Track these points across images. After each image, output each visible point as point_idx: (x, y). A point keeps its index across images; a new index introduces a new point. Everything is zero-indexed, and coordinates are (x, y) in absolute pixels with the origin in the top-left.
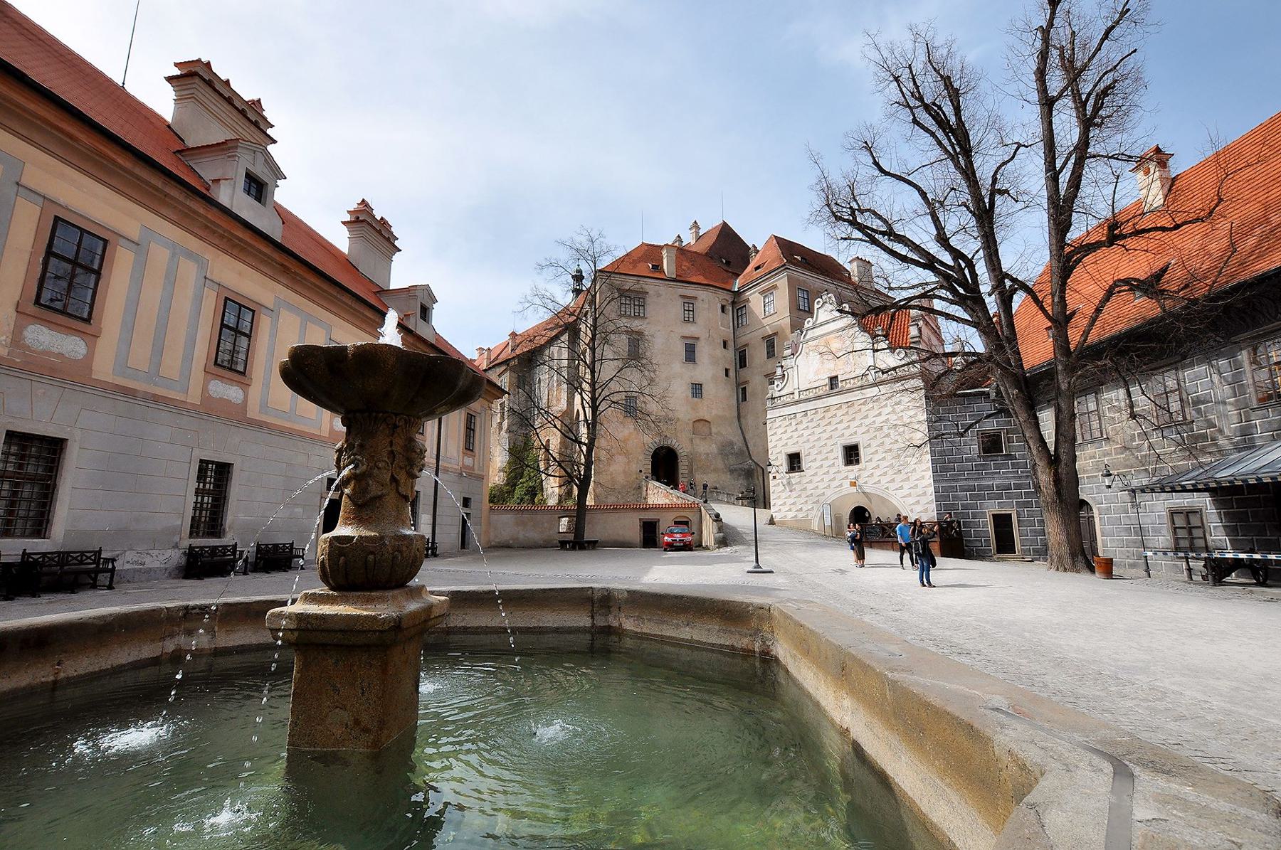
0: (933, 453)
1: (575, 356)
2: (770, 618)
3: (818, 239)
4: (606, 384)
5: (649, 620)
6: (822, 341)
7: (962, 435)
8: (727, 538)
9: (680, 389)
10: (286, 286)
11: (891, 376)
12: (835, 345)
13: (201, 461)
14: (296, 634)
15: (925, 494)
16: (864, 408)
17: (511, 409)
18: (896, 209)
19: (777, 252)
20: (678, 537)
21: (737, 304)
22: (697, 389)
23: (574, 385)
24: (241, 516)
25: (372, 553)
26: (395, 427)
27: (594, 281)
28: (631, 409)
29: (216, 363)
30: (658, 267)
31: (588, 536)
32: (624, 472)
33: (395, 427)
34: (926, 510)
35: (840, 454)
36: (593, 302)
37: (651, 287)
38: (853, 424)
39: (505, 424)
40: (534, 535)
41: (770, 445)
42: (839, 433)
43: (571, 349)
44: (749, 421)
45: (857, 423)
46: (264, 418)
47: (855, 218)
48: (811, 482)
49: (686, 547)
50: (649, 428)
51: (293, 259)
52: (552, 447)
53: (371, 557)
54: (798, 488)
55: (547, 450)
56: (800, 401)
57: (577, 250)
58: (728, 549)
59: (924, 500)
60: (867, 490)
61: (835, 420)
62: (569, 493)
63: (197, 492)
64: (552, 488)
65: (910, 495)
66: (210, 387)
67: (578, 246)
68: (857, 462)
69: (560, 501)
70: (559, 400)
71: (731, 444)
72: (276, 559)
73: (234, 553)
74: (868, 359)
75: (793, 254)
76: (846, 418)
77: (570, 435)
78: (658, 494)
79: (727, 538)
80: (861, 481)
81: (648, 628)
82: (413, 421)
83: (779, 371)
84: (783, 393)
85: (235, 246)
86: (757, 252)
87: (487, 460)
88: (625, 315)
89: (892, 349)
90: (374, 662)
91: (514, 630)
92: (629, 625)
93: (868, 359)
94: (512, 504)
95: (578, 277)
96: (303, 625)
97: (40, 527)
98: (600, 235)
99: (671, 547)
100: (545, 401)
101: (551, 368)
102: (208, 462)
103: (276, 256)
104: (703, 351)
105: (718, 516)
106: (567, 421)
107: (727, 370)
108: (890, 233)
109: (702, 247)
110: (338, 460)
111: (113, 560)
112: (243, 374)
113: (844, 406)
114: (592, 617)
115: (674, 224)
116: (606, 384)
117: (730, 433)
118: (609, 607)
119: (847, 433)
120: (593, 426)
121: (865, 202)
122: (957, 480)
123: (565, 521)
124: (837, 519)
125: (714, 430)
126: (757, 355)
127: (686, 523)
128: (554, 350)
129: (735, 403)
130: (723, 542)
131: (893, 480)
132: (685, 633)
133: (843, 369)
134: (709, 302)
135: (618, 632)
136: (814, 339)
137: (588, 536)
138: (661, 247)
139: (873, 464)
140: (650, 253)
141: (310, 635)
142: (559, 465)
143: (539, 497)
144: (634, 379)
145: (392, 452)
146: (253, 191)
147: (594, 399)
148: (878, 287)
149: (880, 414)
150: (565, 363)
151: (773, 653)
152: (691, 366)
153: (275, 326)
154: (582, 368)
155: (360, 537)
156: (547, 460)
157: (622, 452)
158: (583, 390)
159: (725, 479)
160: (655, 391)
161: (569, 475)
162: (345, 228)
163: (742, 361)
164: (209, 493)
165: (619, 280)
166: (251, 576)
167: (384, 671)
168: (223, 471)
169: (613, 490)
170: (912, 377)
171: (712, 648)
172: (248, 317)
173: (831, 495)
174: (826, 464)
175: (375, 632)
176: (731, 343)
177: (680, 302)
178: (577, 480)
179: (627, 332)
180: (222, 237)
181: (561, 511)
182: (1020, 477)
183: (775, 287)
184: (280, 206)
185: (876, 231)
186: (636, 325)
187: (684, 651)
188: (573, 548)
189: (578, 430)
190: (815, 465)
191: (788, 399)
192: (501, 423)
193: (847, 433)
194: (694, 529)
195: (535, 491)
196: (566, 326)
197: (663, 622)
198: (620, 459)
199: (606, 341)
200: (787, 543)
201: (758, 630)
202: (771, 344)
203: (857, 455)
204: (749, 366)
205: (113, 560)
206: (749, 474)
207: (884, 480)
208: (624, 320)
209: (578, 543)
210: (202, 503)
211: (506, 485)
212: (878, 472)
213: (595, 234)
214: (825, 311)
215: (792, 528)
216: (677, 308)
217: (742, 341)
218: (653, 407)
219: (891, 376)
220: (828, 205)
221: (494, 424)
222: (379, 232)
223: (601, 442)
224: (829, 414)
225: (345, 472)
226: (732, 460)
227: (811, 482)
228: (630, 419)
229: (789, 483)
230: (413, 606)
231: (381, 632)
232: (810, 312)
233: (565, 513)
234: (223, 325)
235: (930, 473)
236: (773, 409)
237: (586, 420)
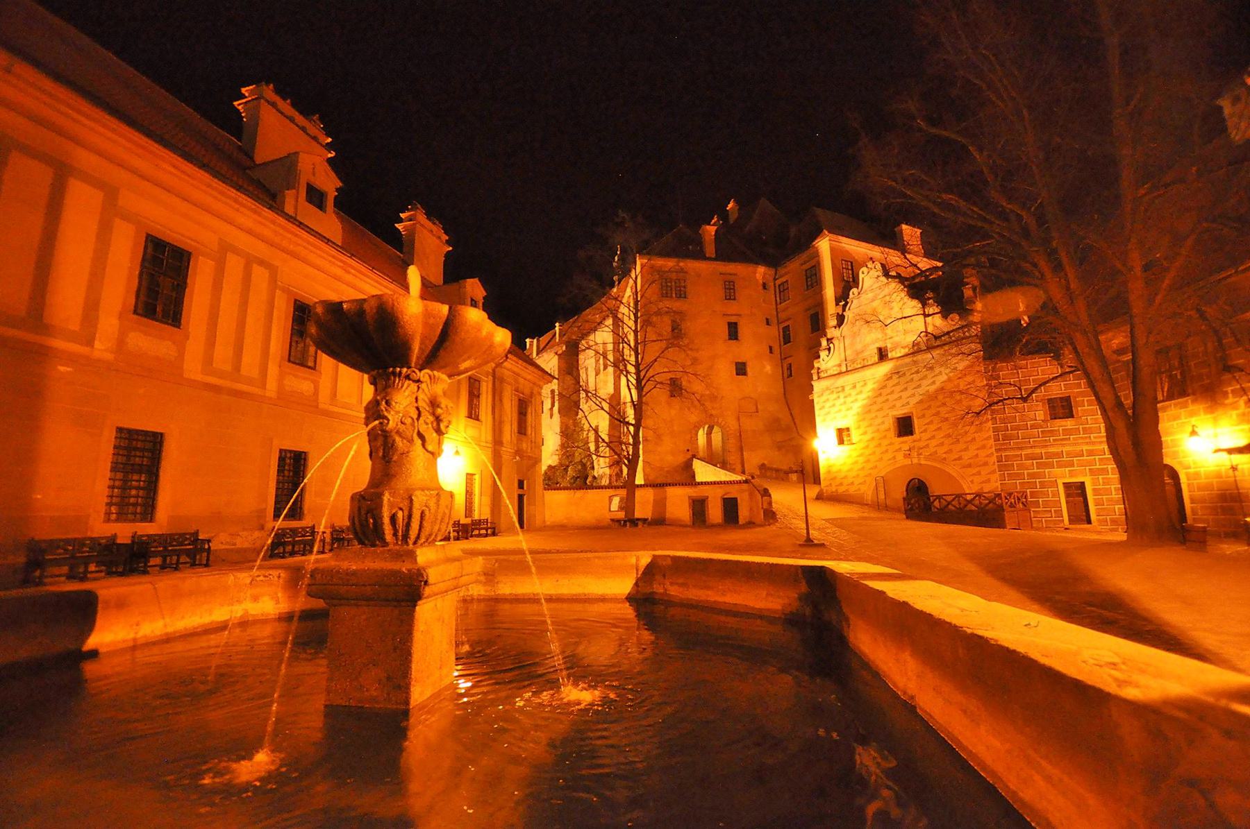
2: (906, 512)
7: (1025, 400)
13: (281, 451)
23: (619, 365)
43: (615, 333)
45: (909, 392)
52: (600, 429)
66: (286, 382)
76: (898, 388)
77: (617, 418)
87: (538, 444)
91: (550, 599)
92: (674, 591)
97: (148, 512)
101: (597, 352)
104: (744, 330)
106: (614, 403)
107: (771, 348)
111: (209, 541)
120: (638, 407)
122: (1021, 449)
147: (638, 380)
150: (610, 347)
154: (626, 351)
156: (597, 442)
158: (628, 372)
182: (1093, 443)
205: (209, 541)
218: (697, 387)
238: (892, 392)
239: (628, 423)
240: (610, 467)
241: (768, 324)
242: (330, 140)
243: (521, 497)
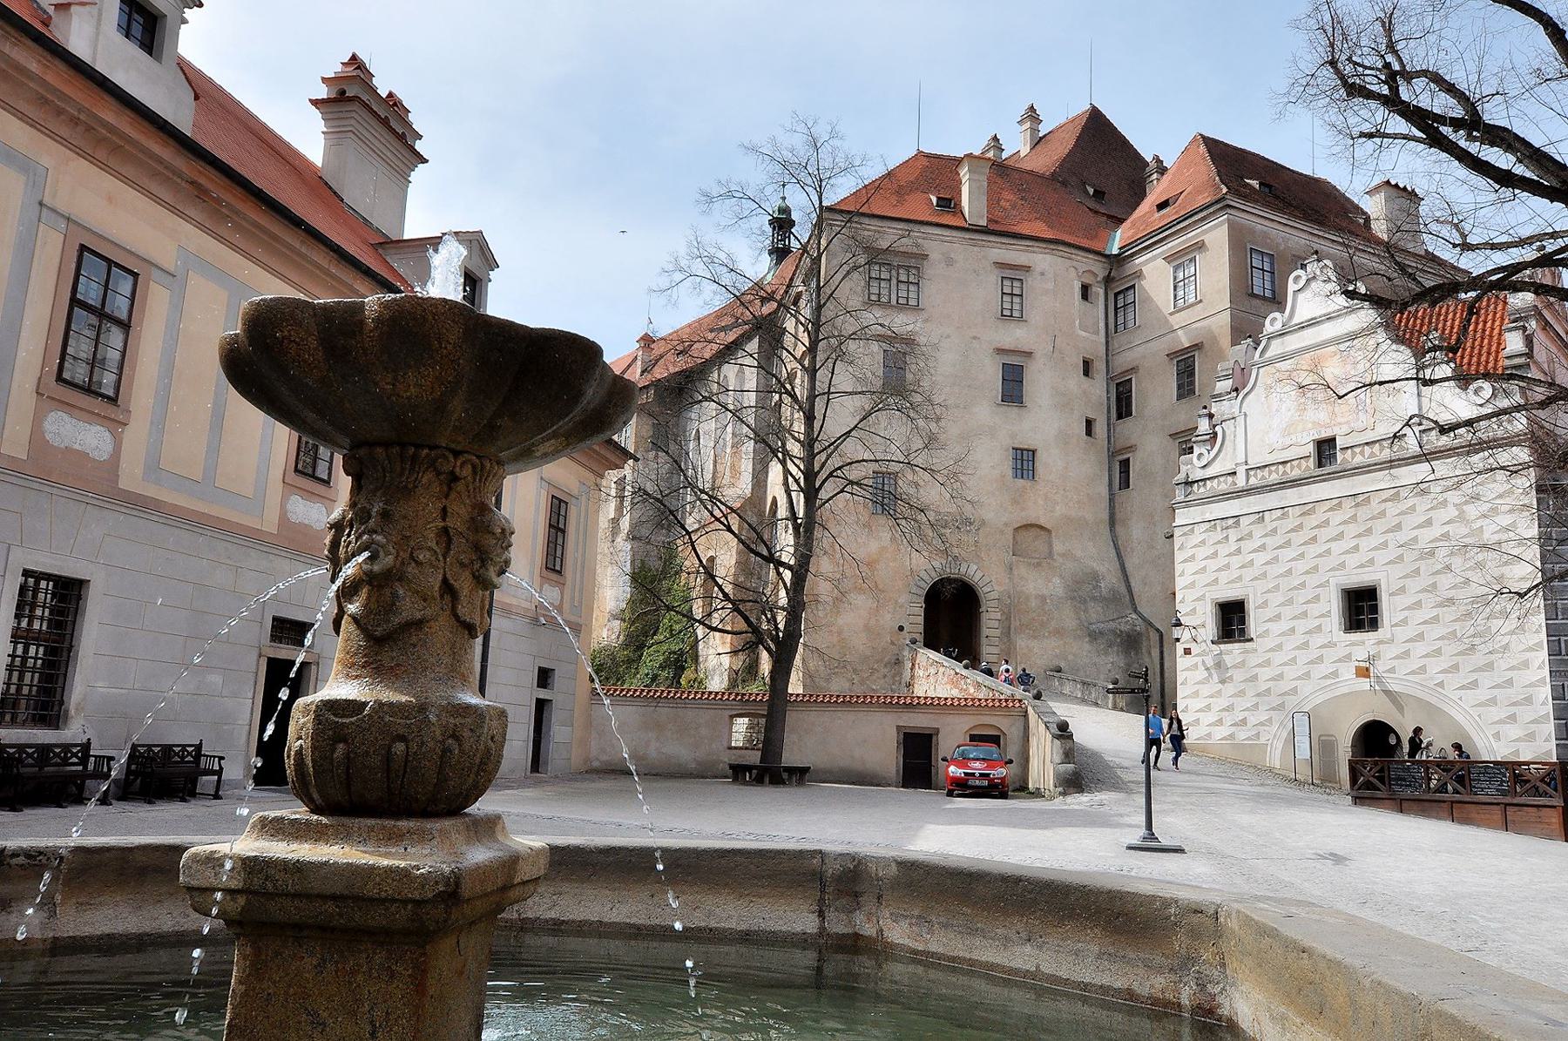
0: (1551, 612)
1: (773, 383)
3: (1306, 142)
4: (835, 444)
5: (945, 926)
6: (1305, 361)
8: (1081, 774)
9: (989, 459)
10: (200, 226)
11: (1460, 439)
12: (1333, 370)
13: (27, 573)
14: (242, 900)
15: (1528, 700)
16: (1392, 509)
17: (640, 491)
18: (1491, 66)
19: (1206, 169)
20: (977, 767)
21: (1115, 285)
22: (1024, 461)
23: (768, 444)
24: (102, 687)
25: (402, 738)
26: (454, 478)
27: (818, 227)
28: (885, 497)
29: (60, 378)
30: (949, 203)
31: (791, 756)
32: (867, 628)
33: (454, 478)
34: (1531, 737)
35: (1334, 606)
36: (815, 270)
37: (937, 245)
38: (1366, 544)
39: (625, 524)
40: (680, 751)
41: (1180, 583)
42: (1333, 561)
44: (1135, 531)
45: (1374, 540)
46: (151, 491)
47: (1395, 90)
48: (1268, 663)
49: (995, 790)
50: (922, 537)
51: (215, 165)
52: (720, 572)
53: (399, 748)
54: (1238, 676)
55: (711, 576)
57: (784, 165)
58: (1084, 798)
59: (1526, 714)
60: (1394, 687)
61: (1325, 534)
62: (752, 669)
63: (16, 637)
64: (717, 658)
65: (1493, 701)
67: (788, 155)
68: (1374, 625)
69: (733, 683)
70: (736, 472)
71: (1095, 577)
72: (165, 775)
73: (84, 761)
74: (1407, 400)
75: (1242, 175)
76: (1352, 530)
77: (757, 547)
78: (936, 677)
79: (1081, 774)
80: (1380, 668)
81: (940, 942)
82: (488, 472)
83: (1204, 426)
84: (1210, 472)
85: (101, 141)
86: (1162, 170)
88: (878, 303)
89: (1463, 379)
90: (399, 968)
92: (899, 933)
93: (1407, 400)
94: (635, 683)
95: (783, 223)
96: (257, 882)
98: (833, 134)
99: (962, 788)
100: (708, 476)
102: (40, 576)
103: (181, 162)
104: (1040, 382)
105: (1063, 727)
106: (753, 520)
107: (1089, 424)
108: (1473, 123)
109: (1045, 162)
110: (335, 545)
112: (113, 400)
113: (1350, 503)
114: (821, 914)
115: (984, 113)
116: (835, 444)
117: (1093, 555)
118: (856, 895)
119: (1352, 560)
120: (806, 530)
121: (1415, 55)
123: (741, 724)
124: (1325, 747)
125: (1058, 547)
126: (1156, 391)
127: (995, 740)
128: (730, 371)
130: (1074, 783)
131: (1455, 668)
132: (1024, 958)
133: (1351, 423)
134: (1055, 276)
135: (878, 949)
136: (1283, 358)
137: (791, 756)
138: (958, 161)
139: (1410, 631)
140: (933, 174)
141: (270, 908)
142: (736, 609)
143: (688, 675)
144: (893, 433)
145: (445, 530)
146: (137, 29)
147: (810, 475)
149: (1429, 523)
150: (751, 399)
151: (1225, 1011)
152: (1013, 411)
153: (178, 307)
154: (786, 411)
155: (380, 704)
156: (708, 597)
157: (866, 588)
158: (786, 453)
159: (1081, 652)
160: (940, 460)
161: (755, 630)
162: (316, 114)
163: (1123, 404)
164: (37, 638)
165: (869, 229)
166: (117, 808)
167: (420, 988)
168: (69, 591)
169: (843, 664)
170: (1510, 442)
171: (1084, 993)
172: (125, 286)
173: (1312, 695)
174: (1302, 626)
175: (405, 902)
176: (1099, 366)
177: (993, 278)
178: (773, 639)
179: (880, 338)
180: (75, 121)
181: (733, 702)
183: (1200, 246)
184: (189, 65)
185: (1441, 119)
186: (901, 322)
187: (1017, 994)
188: (759, 781)
189: (773, 536)
190: (1277, 628)
191: (1223, 486)
192: (615, 522)
193: (1352, 560)
194: (1012, 752)
195: (682, 661)
196: (756, 324)
197: (973, 932)
198: (861, 602)
199: (840, 355)
200: (1212, 792)
201: (1188, 961)
202: (1186, 366)
203: (1375, 609)
204: (1141, 411)
206: (1131, 642)
207: (1435, 666)
208: (878, 312)
209: (767, 770)
210: (24, 658)
211: (625, 646)
212: (1420, 649)
213: (822, 132)
214: (1313, 297)
215: (1222, 761)
216: (987, 289)
217: (1122, 361)
218: (932, 494)
219: (1460, 439)
220: (1333, 63)
221: (604, 522)
222: (385, 122)
223: (822, 565)
224: (1313, 521)
225: (349, 570)
226: (1095, 612)
227: (1268, 663)
228: (882, 520)
229: (1219, 665)
230: (479, 855)
231: (418, 903)
232: (1277, 300)
233: (744, 706)
234: (75, 302)
235: (1544, 655)
236: (1187, 504)
237: (793, 515)
238: (1340, 536)
239: (779, 563)
240: (734, 652)
241: (1086, 373)
242: (206, 931)
243: (541, 705)
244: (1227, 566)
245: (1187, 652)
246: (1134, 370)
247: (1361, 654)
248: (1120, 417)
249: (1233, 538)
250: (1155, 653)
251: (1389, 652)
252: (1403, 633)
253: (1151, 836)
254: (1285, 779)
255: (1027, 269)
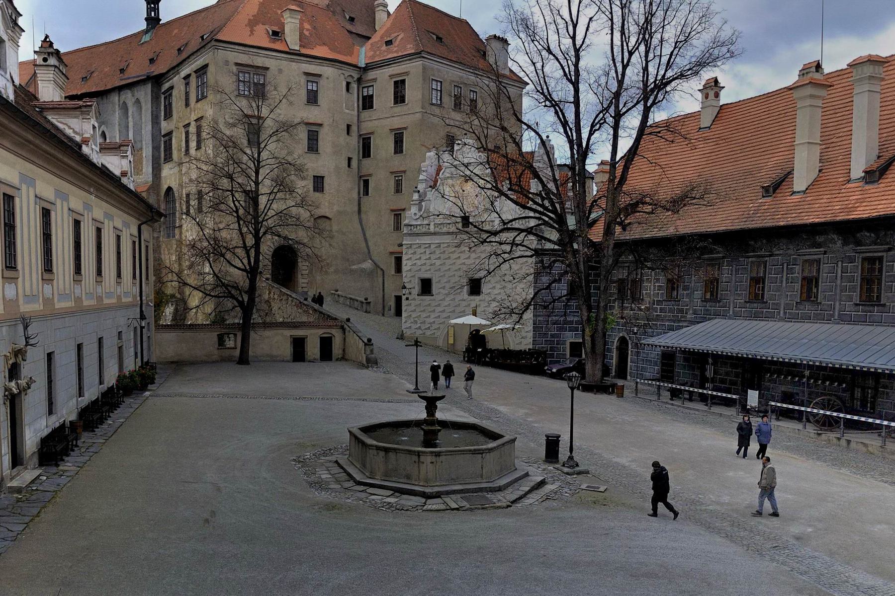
35: (435, 288)
56: (435, 234)
107: (350, 159)
129: (355, 196)
148: (515, 69)
163: (366, 151)
217: (366, 127)
244: (425, 264)
245: (407, 299)
246: (372, 133)
247: (473, 305)
248: (363, 157)
249: (428, 252)
250: (381, 280)
251: (483, 304)
252: (487, 298)
253: (417, 388)
254: (444, 351)
255: (320, 76)
